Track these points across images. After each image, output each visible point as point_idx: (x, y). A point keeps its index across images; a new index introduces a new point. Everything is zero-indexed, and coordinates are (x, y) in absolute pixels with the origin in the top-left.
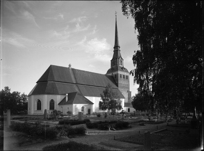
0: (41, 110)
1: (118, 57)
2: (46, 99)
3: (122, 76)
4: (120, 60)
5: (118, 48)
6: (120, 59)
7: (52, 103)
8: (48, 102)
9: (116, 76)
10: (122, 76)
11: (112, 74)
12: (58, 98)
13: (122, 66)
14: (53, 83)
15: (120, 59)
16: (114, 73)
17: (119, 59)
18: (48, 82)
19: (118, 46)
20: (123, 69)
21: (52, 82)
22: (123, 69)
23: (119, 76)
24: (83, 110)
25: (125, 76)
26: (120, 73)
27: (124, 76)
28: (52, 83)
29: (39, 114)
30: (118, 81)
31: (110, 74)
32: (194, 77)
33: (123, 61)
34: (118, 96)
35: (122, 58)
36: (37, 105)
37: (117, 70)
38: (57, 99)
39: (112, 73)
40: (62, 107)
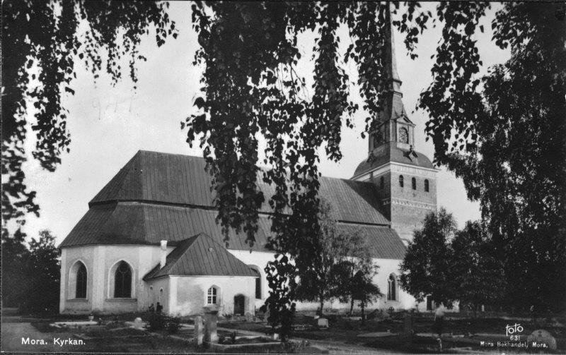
0: (85, 296)
1: (393, 116)
2: (102, 260)
3: (408, 182)
4: (399, 126)
5: (395, 84)
6: (400, 123)
7: (123, 273)
8: (107, 267)
9: (385, 181)
10: (408, 182)
11: (372, 176)
12: (144, 258)
13: (407, 148)
14: (135, 207)
15: (400, 123)
16: (378, 173)
17: (395, 121)
18: (120, 203)
19: (395, 77)
20: (411, 156)
21: (134, 203)
22: (411, 156)
23: (394, 181)
24: (214, 298)
25: (417, 182)
26: (396, 169)
27: (414, 180)
28: (133, 208)
29: (78, 310)
30: (390, 200)
31: (366, 178)
32: (27, 15)
33: (411, 128)
34: (363, 246)
35: (407, 119)
36: (75, 282)
37: (385, 159)
38: (141, 261)
39: (372, 173)
40: (151, 288)
